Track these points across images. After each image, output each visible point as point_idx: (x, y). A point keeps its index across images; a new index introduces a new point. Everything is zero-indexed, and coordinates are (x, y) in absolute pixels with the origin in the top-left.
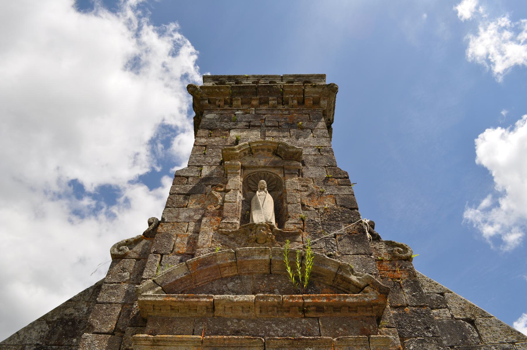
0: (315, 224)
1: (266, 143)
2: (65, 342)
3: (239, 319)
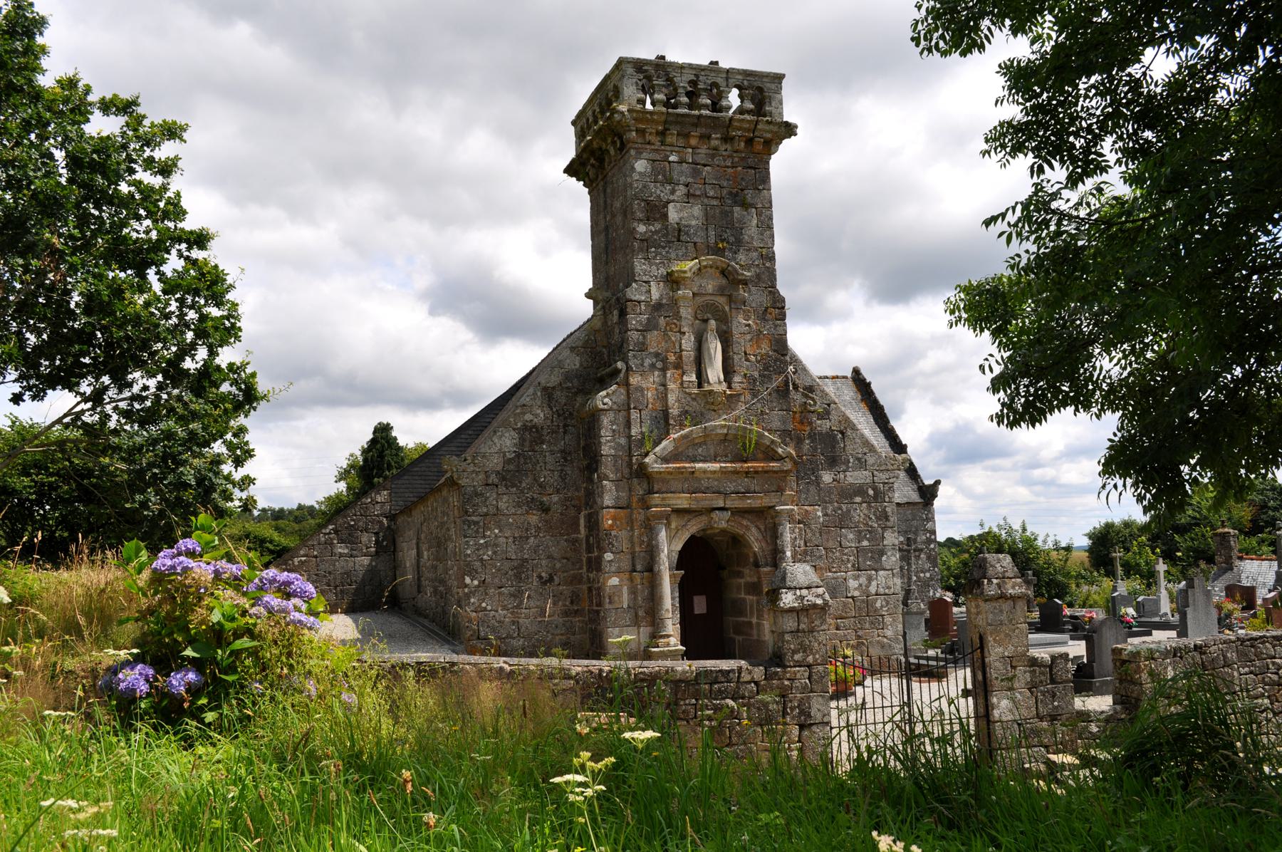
0: (755, 380)
2: (537, 448)
3: (708, 479)
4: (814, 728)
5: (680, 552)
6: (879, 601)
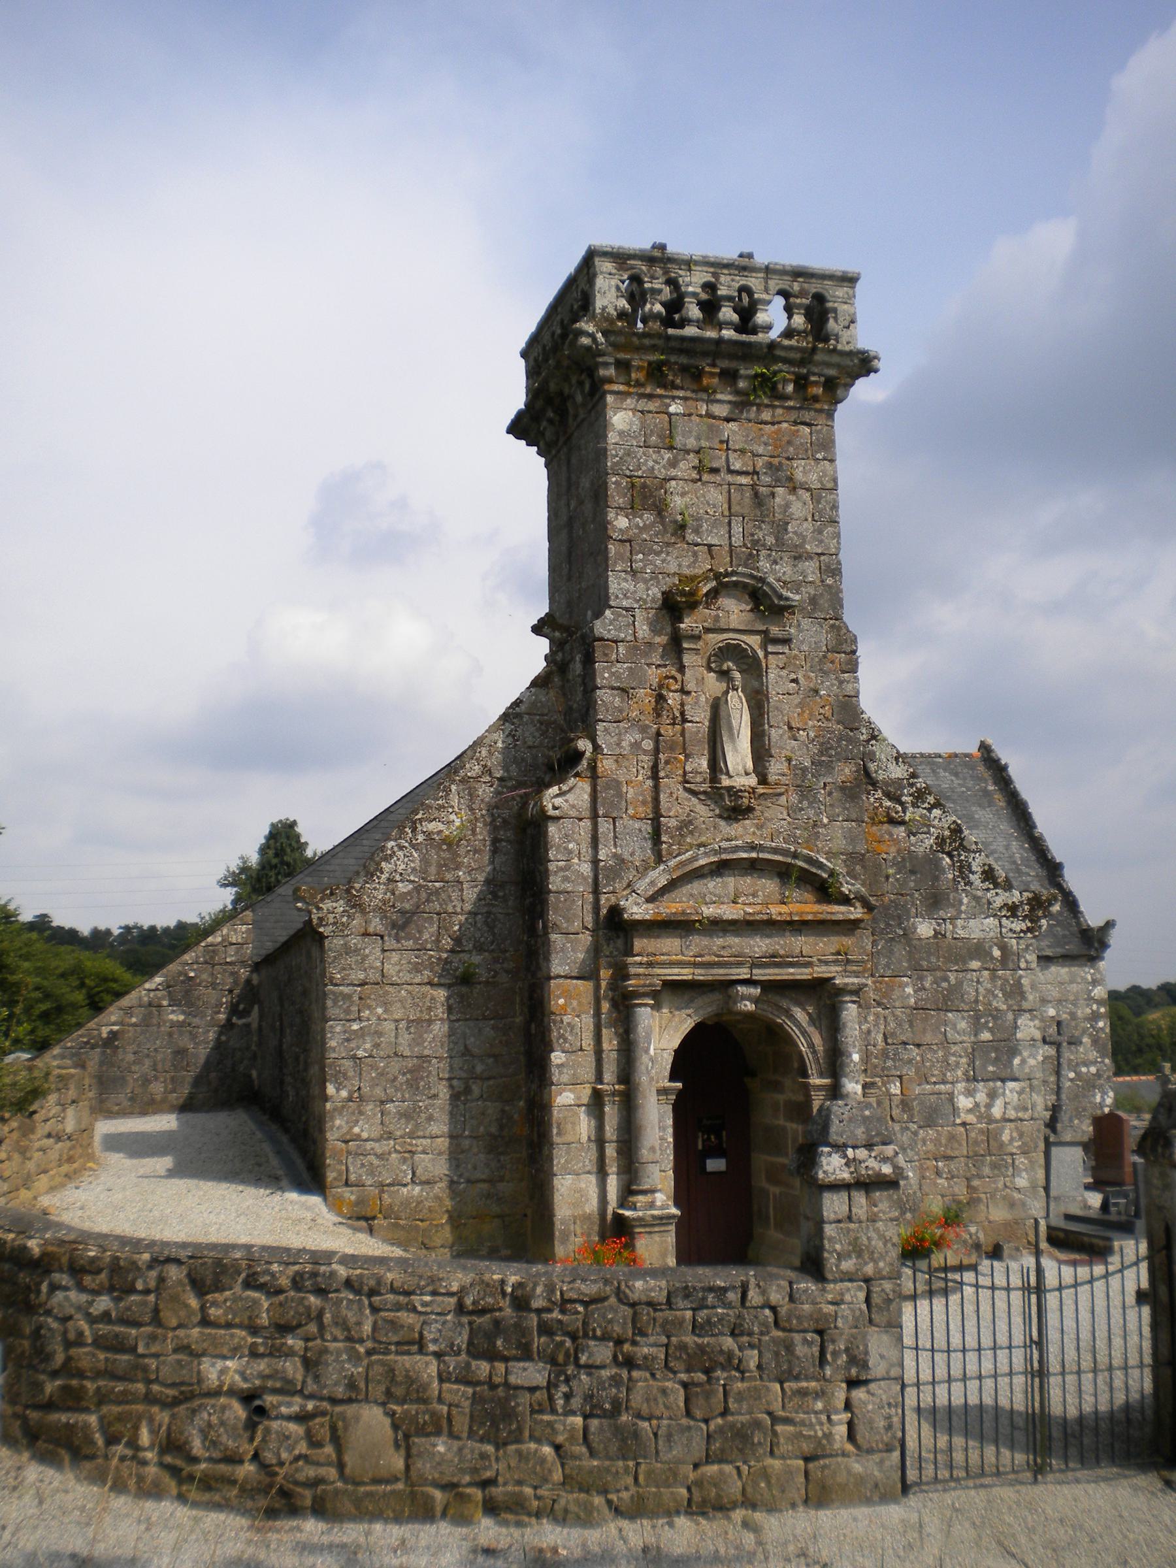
4: (872, 1386)
5: (678, 1052)
6: (1007, 1131)
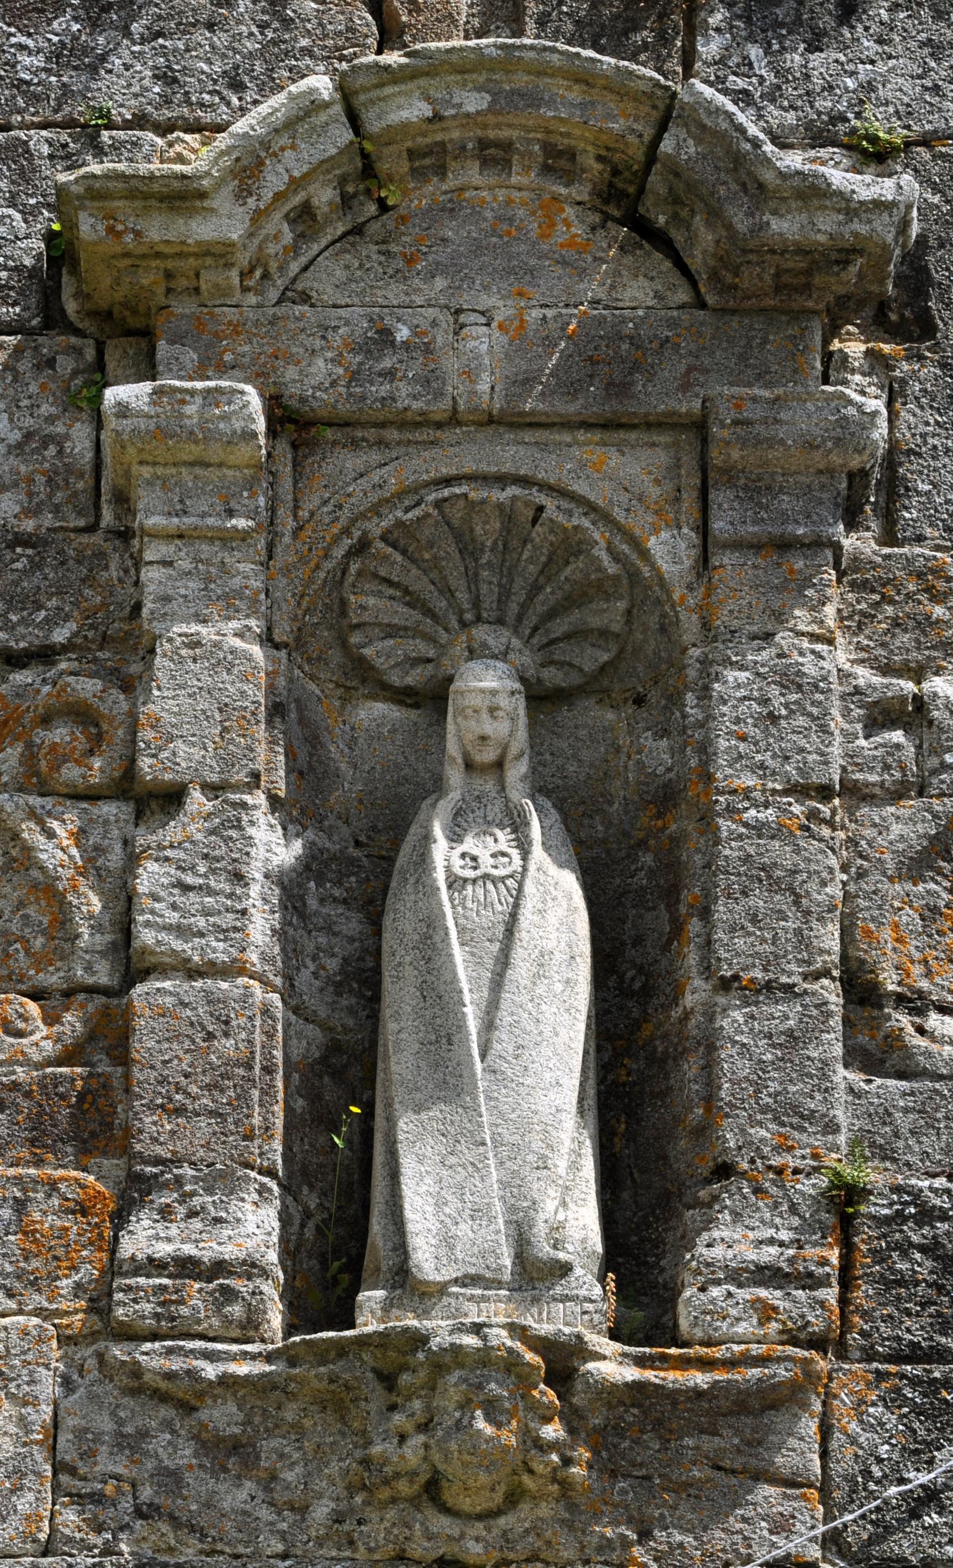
1: (522, 80)
